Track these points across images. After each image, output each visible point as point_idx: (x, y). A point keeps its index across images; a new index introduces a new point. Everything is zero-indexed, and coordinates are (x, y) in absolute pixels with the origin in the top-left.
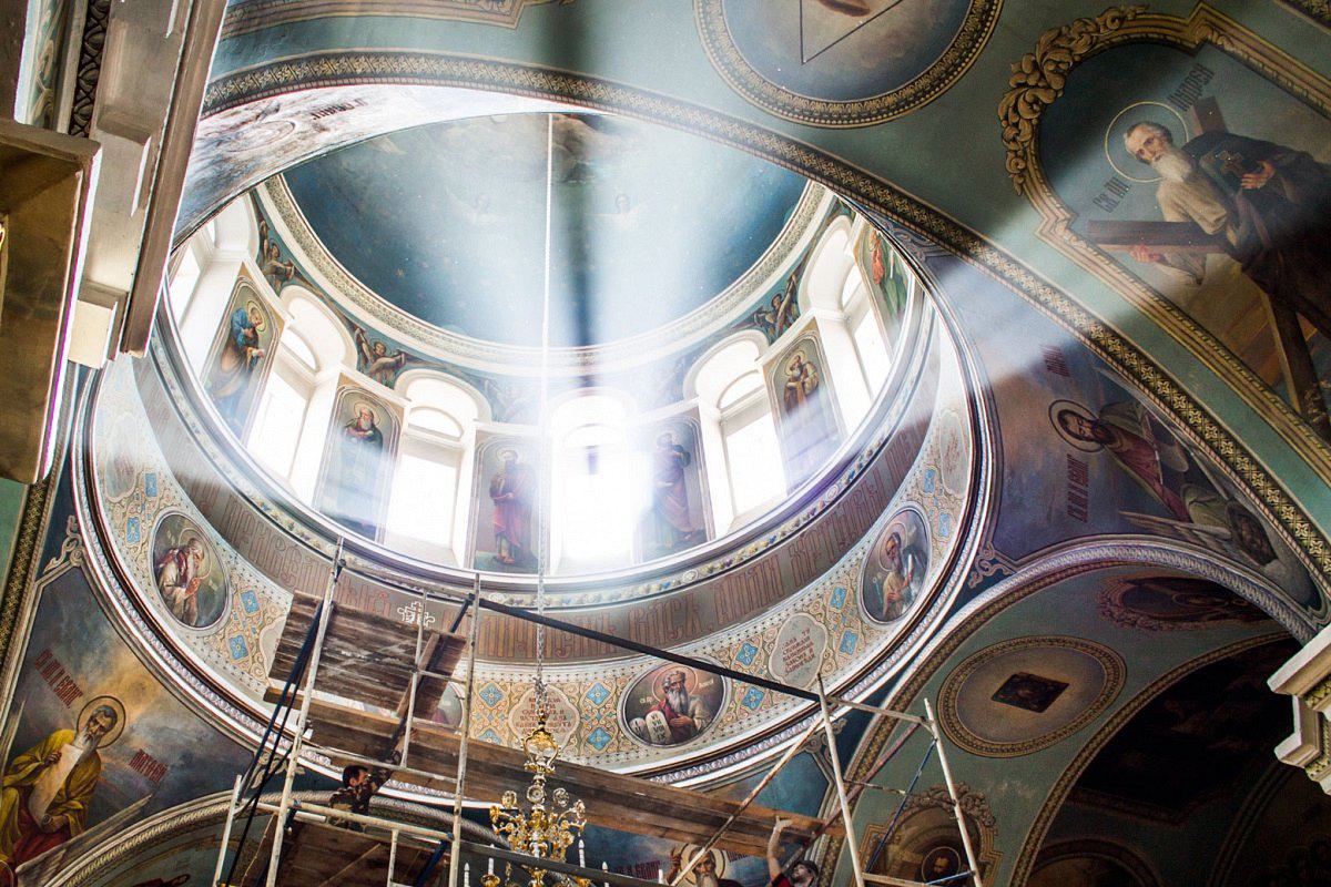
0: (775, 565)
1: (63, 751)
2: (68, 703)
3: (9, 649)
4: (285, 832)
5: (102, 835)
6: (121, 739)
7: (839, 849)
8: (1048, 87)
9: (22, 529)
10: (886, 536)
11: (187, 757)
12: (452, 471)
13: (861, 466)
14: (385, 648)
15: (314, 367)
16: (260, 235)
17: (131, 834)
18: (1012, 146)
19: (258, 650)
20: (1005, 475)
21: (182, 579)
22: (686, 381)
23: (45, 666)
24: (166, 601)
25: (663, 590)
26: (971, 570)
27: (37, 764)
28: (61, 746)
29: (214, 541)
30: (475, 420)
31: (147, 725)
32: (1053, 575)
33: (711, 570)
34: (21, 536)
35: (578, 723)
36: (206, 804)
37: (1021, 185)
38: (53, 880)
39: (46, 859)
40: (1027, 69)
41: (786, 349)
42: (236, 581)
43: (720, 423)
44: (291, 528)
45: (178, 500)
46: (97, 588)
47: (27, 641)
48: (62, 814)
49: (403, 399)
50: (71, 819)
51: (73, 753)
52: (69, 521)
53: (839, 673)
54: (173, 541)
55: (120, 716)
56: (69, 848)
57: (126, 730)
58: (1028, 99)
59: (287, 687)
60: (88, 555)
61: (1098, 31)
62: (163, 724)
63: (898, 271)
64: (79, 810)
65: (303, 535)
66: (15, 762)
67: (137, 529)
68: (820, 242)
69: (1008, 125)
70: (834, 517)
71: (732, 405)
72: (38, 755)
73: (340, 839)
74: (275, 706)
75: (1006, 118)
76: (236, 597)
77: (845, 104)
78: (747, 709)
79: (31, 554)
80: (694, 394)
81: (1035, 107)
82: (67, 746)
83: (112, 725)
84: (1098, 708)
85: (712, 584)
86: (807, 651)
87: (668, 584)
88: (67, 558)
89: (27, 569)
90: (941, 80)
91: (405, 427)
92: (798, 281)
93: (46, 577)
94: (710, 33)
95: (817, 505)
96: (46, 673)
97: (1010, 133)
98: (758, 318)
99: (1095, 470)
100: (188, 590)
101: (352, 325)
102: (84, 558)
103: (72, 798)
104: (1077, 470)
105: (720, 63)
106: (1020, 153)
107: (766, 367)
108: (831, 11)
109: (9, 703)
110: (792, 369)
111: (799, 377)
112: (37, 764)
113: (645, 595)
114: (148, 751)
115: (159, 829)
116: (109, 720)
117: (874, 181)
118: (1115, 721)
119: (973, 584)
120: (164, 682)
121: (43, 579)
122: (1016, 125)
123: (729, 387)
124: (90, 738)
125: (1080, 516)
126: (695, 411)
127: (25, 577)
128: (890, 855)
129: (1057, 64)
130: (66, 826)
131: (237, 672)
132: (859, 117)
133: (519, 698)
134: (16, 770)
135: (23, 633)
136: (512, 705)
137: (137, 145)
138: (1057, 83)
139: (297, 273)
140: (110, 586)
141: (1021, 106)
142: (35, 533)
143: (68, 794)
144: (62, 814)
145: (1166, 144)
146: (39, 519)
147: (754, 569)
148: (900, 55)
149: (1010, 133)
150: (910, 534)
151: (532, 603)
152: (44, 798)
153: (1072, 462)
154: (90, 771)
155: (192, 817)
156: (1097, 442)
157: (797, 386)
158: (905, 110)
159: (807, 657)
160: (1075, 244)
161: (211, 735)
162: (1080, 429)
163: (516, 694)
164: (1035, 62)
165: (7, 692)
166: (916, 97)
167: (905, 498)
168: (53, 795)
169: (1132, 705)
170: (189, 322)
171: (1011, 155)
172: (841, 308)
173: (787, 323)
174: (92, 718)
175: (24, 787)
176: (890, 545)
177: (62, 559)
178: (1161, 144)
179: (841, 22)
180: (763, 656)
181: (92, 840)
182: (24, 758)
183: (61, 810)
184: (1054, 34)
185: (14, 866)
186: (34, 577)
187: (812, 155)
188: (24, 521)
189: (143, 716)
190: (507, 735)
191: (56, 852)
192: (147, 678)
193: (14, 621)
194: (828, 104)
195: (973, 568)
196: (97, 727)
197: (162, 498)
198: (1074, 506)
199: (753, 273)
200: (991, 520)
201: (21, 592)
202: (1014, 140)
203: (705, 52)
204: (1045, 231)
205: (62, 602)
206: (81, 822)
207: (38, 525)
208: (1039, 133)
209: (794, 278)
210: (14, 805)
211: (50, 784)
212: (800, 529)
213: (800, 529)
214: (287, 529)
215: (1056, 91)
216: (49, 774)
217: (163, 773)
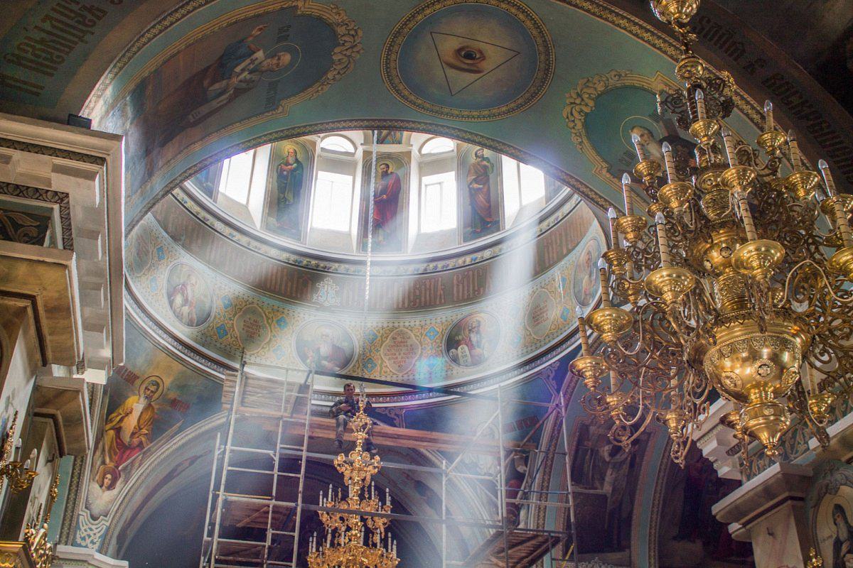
4: (222, 512)
7: (558, 437)
8: (587, 105)
12: (350, 178)
18: (573, 130)
21: (186, 301)
24: (178, 317)
30: (362, 144)
35: (420, 352)
36: (213, 420)
40: (575, 96)
44: (249, 244)
48: (138, 437)
50: (143, 439)
55: (161, 384)
56: (144, 453)
61: (608, 80)
65: (256, 247)
66: (110, 418)
75: (568, 118)
82: (135, 404)
83: (157, 390)
91: (318, 151)
97: (572, 125)
100: (190, 306)
103: (142, 429)
113: (463, 265)
120: (183, 363)
122: (573, 121)
128: (591, 432)
129: (590, 94)
130: (141, 443)
133: (387, 338)
136: (383, 342)
137: (99, 333)
138: (591, 103)
141: (575, 114)
143: (139, 427)
144: (138, 437)
145: (651, 138)
149: (572, 125)
160: (613, 180)
163: (385, 335)
164: (577, 93)
171: (573, 135)
174: (146, 388)
178: (649, 138)
183: (137, 435)
184: (586, 80)
185: (117, 467)
190: (380, 362)
191: (138, 457)
202: (573, 128)
204: (597, 172)
208: (585, 125)
210: (112, 439)
211: (129, 424)
214: (246, 246)
215: (592, 107)
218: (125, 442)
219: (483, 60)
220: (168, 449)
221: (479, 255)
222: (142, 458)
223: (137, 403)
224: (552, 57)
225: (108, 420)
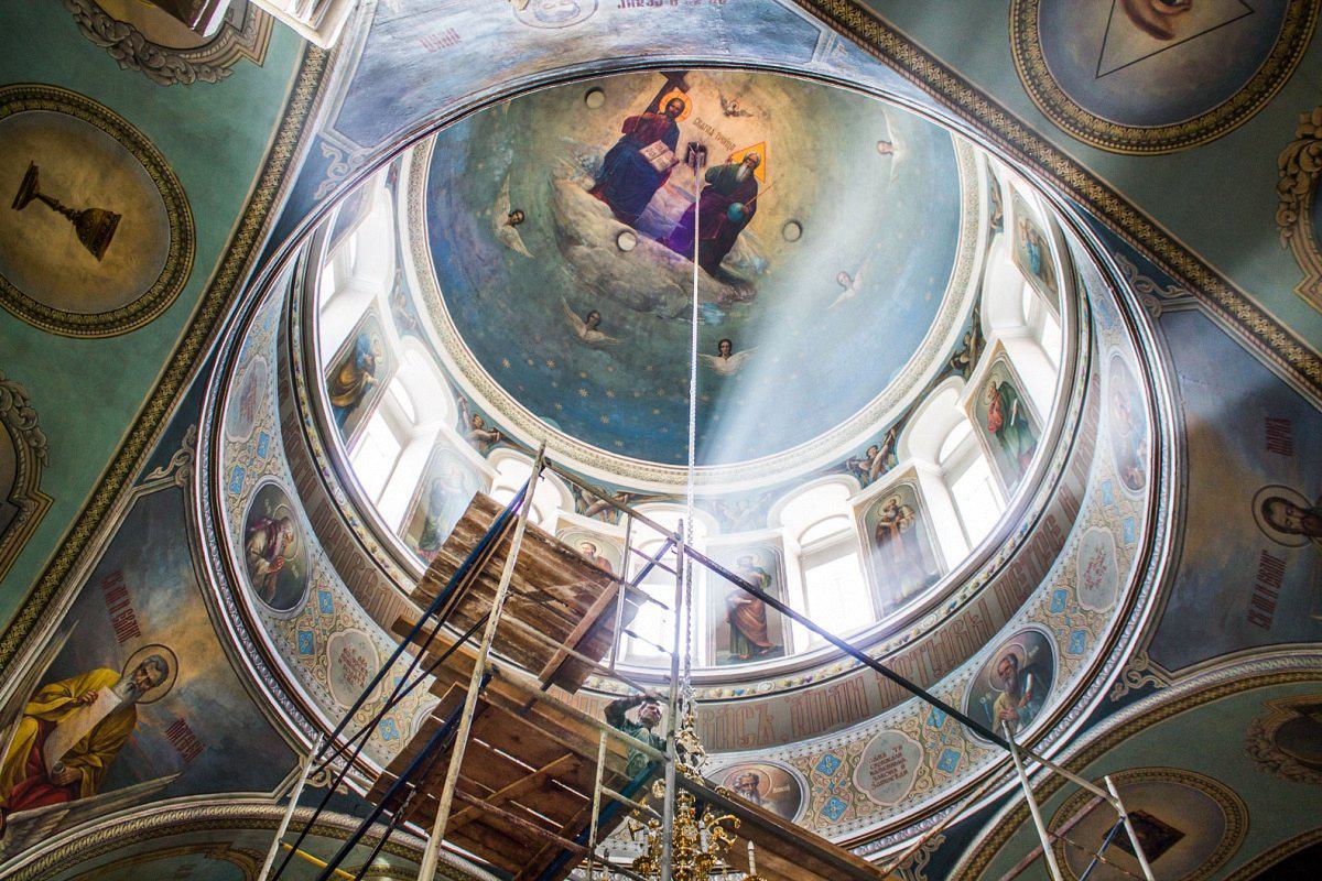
0: (860, 685)
1: (100, 693)
2: (123, 640)
3: (73, 569)
5: (114, 804)
6: (166, 701)
9: (140, 421)
10: (999, 656)
11: (229, 744)
13: (964, 597)
14: (556, 587)
15: (413, 420)
16: (395, 279)
17: (145, 813)
18: (1286, 198)
19: (324, 653)
20: (1179, 575)
21: (268, 553)
22: (771, 513)
23: (111, 589)
25: (736, 696)
26: (1116, 681)
27: (68, 699)
28: (100, 687)
29: (304, 528)
31: (197, 692)
32: (1217, 688)
33: (789, 684)
34: (136, 428)
36: (233, 801)
37: (1288, 238)
38: (47, 841)
39: (46, 814)
41: (880, 494)
42: (316, 577)
43: (800, 558)
44: (374, 551)
45: (281, 474)
46: (192, 519)
47: (103, 552)
49: (494, 471)
50: (86, 776)
51: (110, 700)
52: (189, 430)
53: (936, 790)
54: (269, 510)
55: (172, 673)
57: (173, 691)
58: (1311, 151)
59: (424, 619)
60: (194, 478)
62: (213, 697)
63: (1021, 418)
64: (97, 768)
66: (46, 689)
67: (241, 480)
68: (925, 401)
69: (1286, 175)
70: (930, 645)
71: (808, 545)
72: (73, 690)
73: (523, 739)
74: (402, 639)
75: (1285, 168)
76: (313, 592)
77: (1127, 129)
78: (827, 818)
79: (140, 452)
80: (778, 524)
81: (1317, 161)
82: (106, 689)
83: (160, 681)
84: (1208, 870)
85: (787, 697)
86: (898, 767)
87: (742, 692)
88: (173, 473)
89: (130, 468)
90: (1227, 120)
92: (897, 435)
93: (146, 486)
94: (1021, 22)
95: (911, 632)
96: (111, 598)
97: (1287, 184)
98: (851, 466)
99: (1294, 570)
100: (271, 566)
101: (457, 392)
102: (190, 479)
103: (93, 752)
104: (1271, 569)
105: (1021, 57)
106: (1293, 205)
107: (857, 508)
108: (1135, 28)
109: (63, 616)
110: (886, 511)
111: (894, 518)
112: (68, 699)
114: (189, 723)
115: (178, 816)
116: (159, 674)
117: (1138, 215)
118: (1267, 858)
119: (1115, 697)
121: (142, 487)
122: (1294, 176)
123: (813, 525)
124: (132, 687)
125: (1261, 623)
126: (779, 540)
127: (126, 476)
130: (78, 782)
131: (300, 668)
132: (1138, 145)
134: (44, 699)
135: (102, 541)
139: (417, 328)
140: (204, 522)
141: (1304, 158)
142: (153, 429)
143: (90, 745)
144: (77, 767)
146: (162, 413)
147: (836, 688)
148: (1193, 88)
149: (1287, 184)
150: (1031, 655)
151: (598, 686)
152: (62, 743)
153: (1266, 558)
154: (121, 727)
155: (217, 811)
156: (1304, 534)
157: (890, 522)
158: (1184, 146)
159: (898, 773)
161: (260, 725)
162: (1287, 520)
165: (64, 602)
166: (1199, 134)
167: (1025, 619)
168: (75, 741)
169: (1279, 852)
170: (328, 312)
171: (1283, 207)
172: (937, 461)
173: (882, 470)
175: (46, 721)
176: (1003, 665)
177: (167, 472)
179: (1144, 42)
180: (847, 769)
181: (102, 808)
182: (56, 688)
185: (7, 811)
186: (134, 481)
187: (1082, 176)
188: (144, 413)
189: (196, 681)
192: (212, 639)
193: (97, 523)
194: (1111, 124)
195: (1119, 679)
196: (144, 678)
197: (269, 463)
198: (1257, 610)
199: (852, 423)
200: (1151, 626)
201: (116, 492)
202: (1289, 191)
203: (1010, 41)
205: (152, 521)
206: (95, 783)
207: (158, 420)
209: (893, 432)
212: (890, 654)
213: (890, 654)
216: (78, 714)
217: (199, 751)
218: (47, 763)
219: (1186, 10)
220: (125, 823)
221: (747, 688)
222: (66, 816)
223: (112, 688)
224: (1308, 33)
225: (39, 694)
